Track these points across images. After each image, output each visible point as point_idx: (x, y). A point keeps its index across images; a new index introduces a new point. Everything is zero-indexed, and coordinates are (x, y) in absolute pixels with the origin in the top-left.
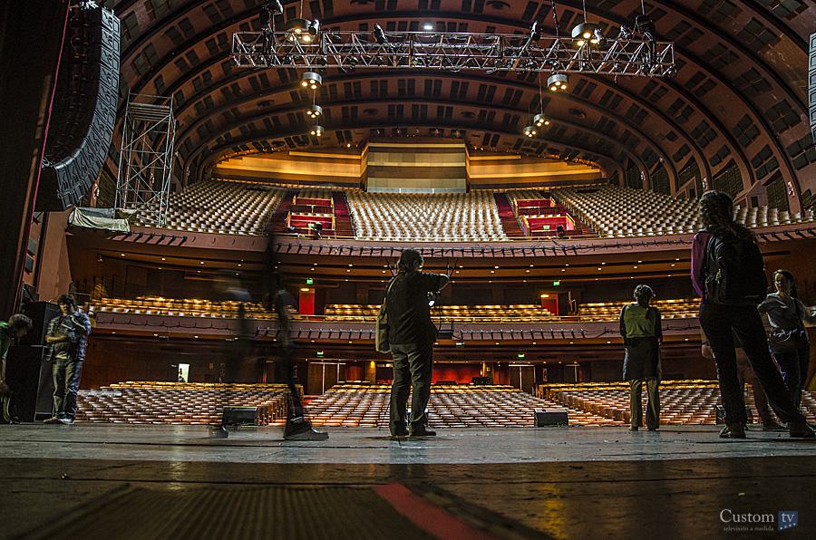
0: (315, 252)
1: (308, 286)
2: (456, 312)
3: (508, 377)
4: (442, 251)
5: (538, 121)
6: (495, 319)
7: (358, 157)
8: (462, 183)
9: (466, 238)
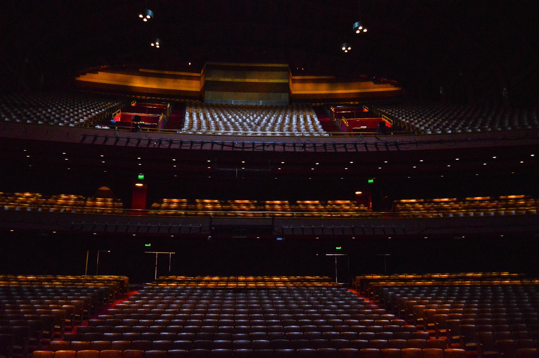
0: (133, 144)
1: (140, 181)
2: (278, 207)
3: (324, 268)
4: (264, 145)
5: (357, 29)
6: (316, 214)
7: (198, 75)
8: (284, 97)
9: (287, 134)
